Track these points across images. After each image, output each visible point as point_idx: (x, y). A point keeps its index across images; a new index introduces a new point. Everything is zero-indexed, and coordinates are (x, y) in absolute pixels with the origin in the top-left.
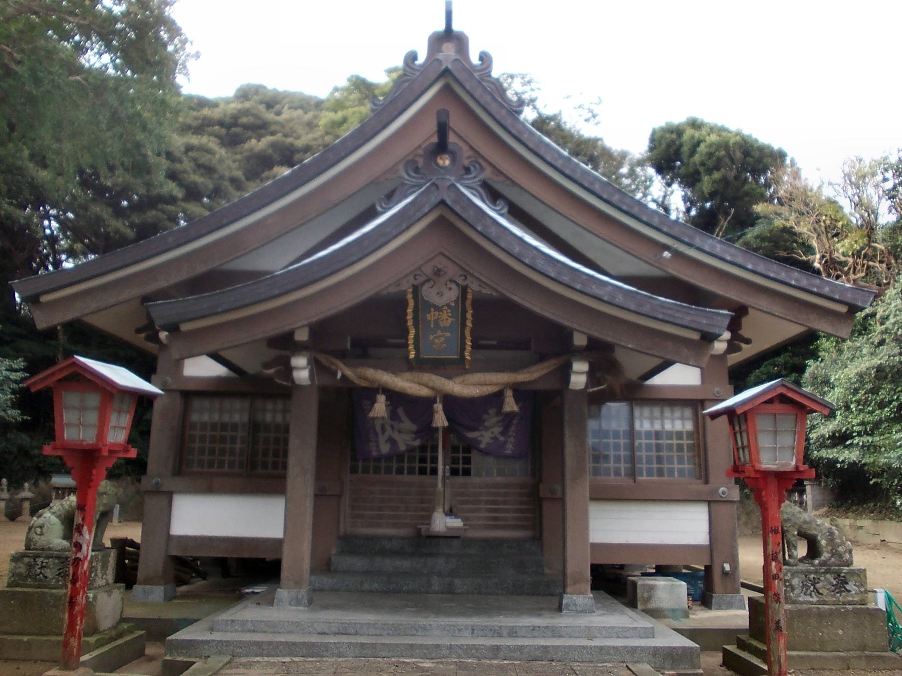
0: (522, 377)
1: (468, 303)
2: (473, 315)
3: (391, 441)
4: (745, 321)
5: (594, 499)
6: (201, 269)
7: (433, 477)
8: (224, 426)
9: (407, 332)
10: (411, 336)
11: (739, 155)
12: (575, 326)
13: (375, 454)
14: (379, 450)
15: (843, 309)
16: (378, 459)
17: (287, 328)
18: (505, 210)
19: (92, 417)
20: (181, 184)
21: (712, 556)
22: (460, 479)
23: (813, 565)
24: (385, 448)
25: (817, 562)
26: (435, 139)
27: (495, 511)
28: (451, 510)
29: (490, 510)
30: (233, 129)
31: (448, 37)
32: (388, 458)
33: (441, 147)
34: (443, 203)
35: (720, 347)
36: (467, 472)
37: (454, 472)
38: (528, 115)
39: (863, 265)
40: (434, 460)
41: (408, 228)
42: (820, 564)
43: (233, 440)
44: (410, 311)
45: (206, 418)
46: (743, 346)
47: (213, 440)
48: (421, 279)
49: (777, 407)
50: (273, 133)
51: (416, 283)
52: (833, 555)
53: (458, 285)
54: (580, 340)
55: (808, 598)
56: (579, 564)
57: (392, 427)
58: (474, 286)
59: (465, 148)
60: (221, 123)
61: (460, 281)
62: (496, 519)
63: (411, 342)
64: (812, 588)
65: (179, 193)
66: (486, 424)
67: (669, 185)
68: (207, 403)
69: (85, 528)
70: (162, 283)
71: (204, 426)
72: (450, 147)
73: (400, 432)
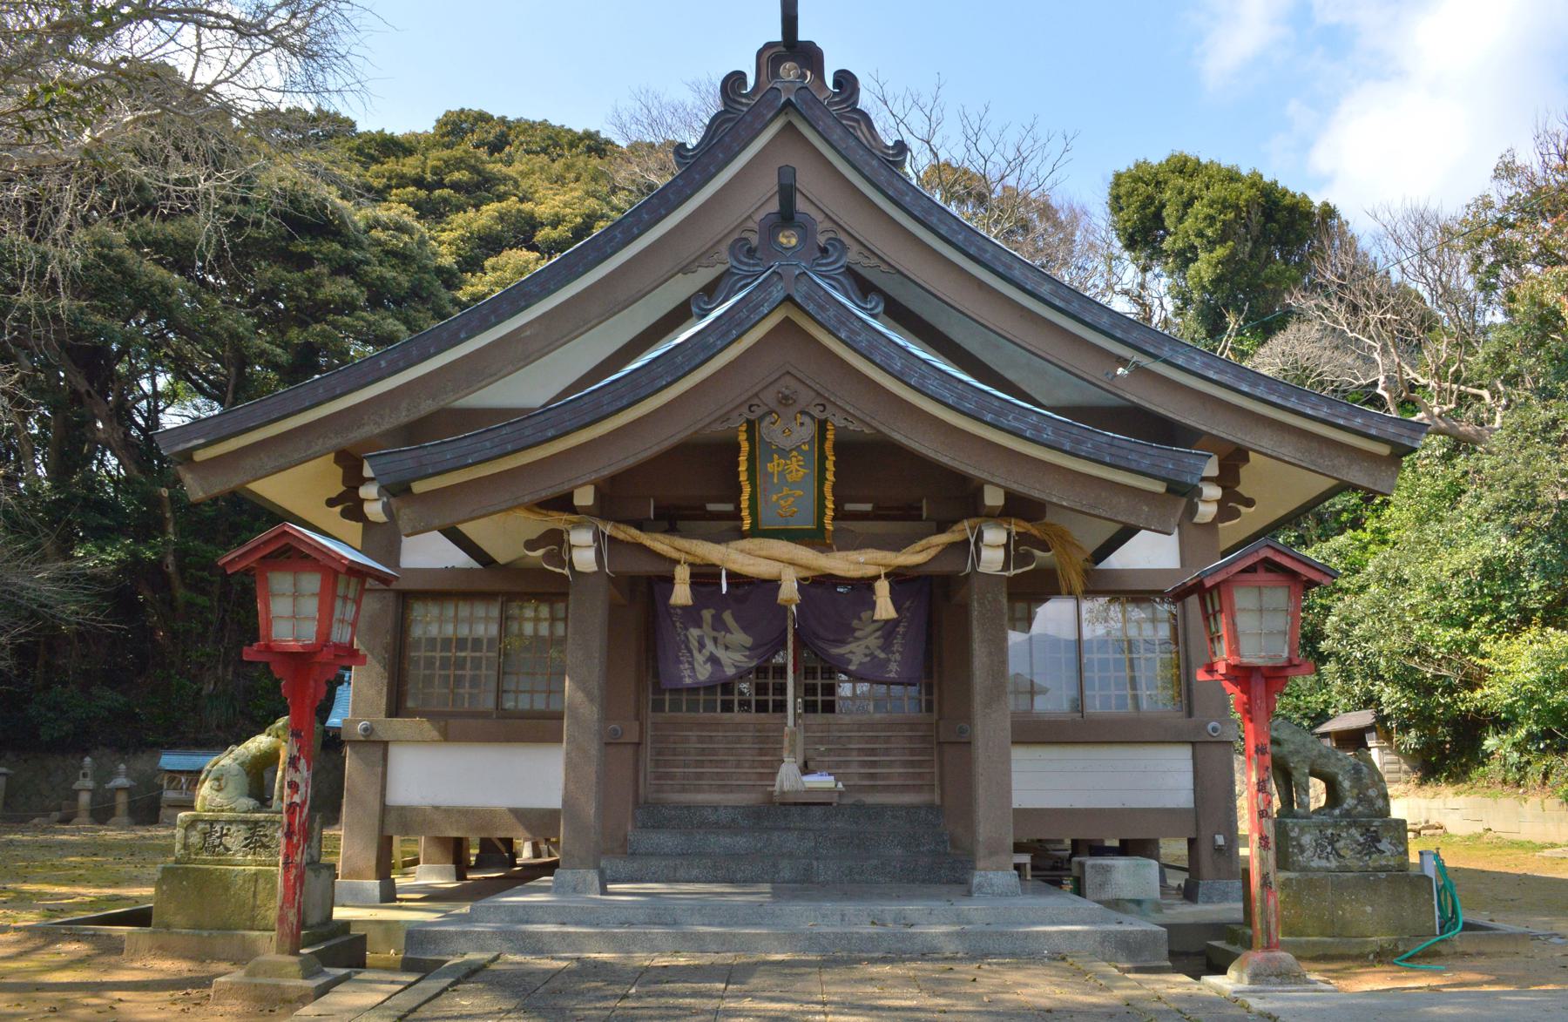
0: (910, 557)
1: (828, 445)
2: (835, 463)
3: (713, 660)
4: (1244, 472)
5: (1018, 741)
6: (427, 407)
7: (778, 715)
8: (461, 643)
9: (740, 490)
10: (745, 497)
11: (1257, 217)
12: (985, 476)
13: (688, 681)
14: (694, 676)
15: (1384, 450)
16: (693, 690)
17: (566, 487)
18: (880, 308)
19: (311, 606)
20: (360, 281)
21: (1197, 825)
22: (819, 718)
23: (1332, 816)
24: (704, 672)
25: (1337, 812)
26: (774, 206)
27: (874, 764)
28: (806, 764)
29: (864, 764)
30: (437, 192)
31: (792, 50)
32: (709, 688)
33: (787, 216)
34: (789, 299)
35: (1207, 511)
36: (829, 707)
37: (810, 707)
38: (917, 165)
39: (1452, 393)
40: (782, 690)
41: (739, 337)
42: (1341, 815)
43: (477, 664)
44: (743, 458)
45: (434, 630)
46: (1243, 509)
47: (445, 663)
48: (759, 412)
49: (1262, 576)
50: (501, 198)
51: (752, 417)
52: (1360, 801)
53: (813, 418)
54: (993, 498)
55: (1324, 863)
56: (990, 827)
57: (715, 640)
58: (837, 420)
59: (819, 217)
60: (419, 182)
61: (816, 412)
62: (872, 776)
63: (745, 504)
64: (1329, 849)
65: (359, 295)
66: (858, 634)
67: (1145, 270)
68: (434, 610)
69: (303, 761)
70: (370, 429)
71: (432, 642)
72: (797, 218)
73: (727, 648)
